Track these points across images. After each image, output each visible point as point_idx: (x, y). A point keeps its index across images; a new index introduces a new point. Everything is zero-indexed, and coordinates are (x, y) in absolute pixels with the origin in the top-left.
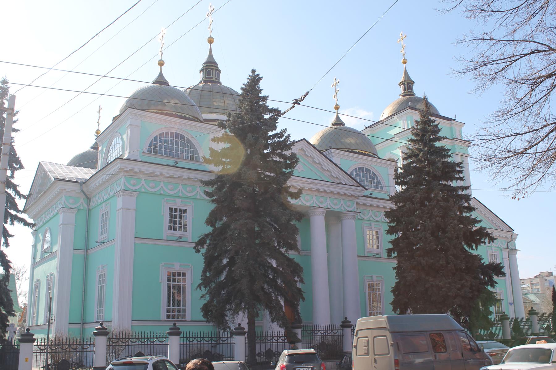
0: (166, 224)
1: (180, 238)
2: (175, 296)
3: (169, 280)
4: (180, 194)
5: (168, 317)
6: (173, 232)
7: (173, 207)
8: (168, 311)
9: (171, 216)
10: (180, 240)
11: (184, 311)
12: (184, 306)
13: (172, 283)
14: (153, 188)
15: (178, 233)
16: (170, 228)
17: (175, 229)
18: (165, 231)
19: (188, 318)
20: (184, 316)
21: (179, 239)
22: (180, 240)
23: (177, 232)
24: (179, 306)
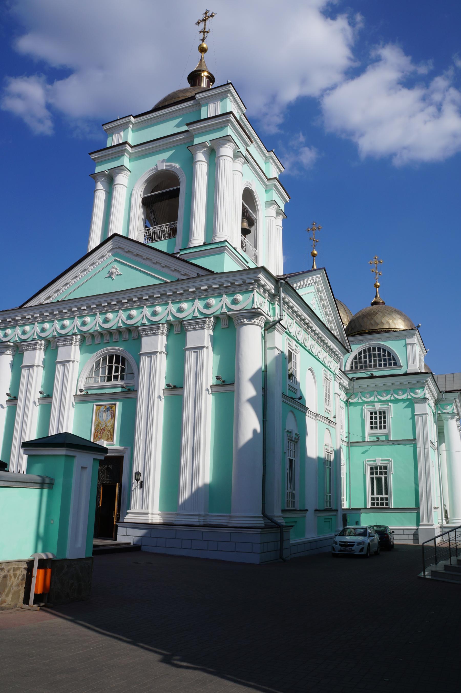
5: (373, 504)
11: (372, 473)
12: (372, 479)
17: (376, 428)
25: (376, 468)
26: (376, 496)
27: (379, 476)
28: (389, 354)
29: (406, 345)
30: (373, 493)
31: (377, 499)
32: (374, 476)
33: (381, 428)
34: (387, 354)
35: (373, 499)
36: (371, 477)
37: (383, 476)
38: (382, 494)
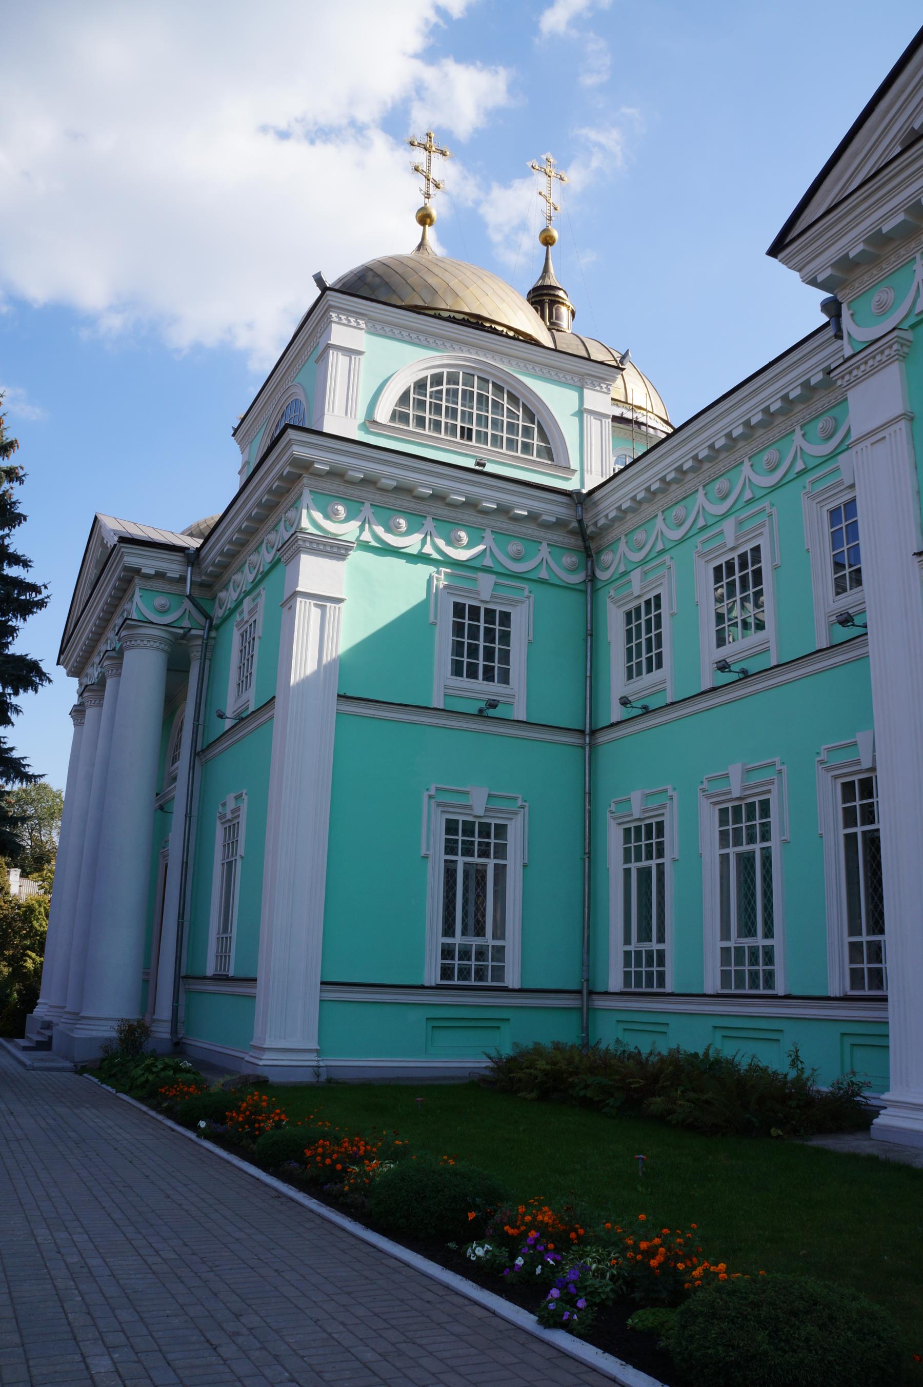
0: (447, 656)
1: (493, 705)
2: (470, 897)
3: (450, 848)
4: (544, 574)
5: (446, 972)
6: (464, 682)
7: (468, 602)
8: (447, 952)
9: (458, 629)
10: (491, 712)
11: (499, 952)
12: (500, 933)
13: (461, 860)
14: (517, 558)
16: (457, 670)
18: (439, 681)
19: (512, 979)
20: (499, 972)
21: (487, 713)
22: (491, 712)
23: (479, 684)
24: (480, 931)
25: (468, 829)
26: (458, 940)
27: (475, 859)
28: (530, 415)
29: (581, 413)
30: (500, 871)
31: (465, 954)
32: (461, 860)
33: (489, 675)
34: (521, 414)
35: (501, 851)
36: (503, 937)
37: (491, 862)
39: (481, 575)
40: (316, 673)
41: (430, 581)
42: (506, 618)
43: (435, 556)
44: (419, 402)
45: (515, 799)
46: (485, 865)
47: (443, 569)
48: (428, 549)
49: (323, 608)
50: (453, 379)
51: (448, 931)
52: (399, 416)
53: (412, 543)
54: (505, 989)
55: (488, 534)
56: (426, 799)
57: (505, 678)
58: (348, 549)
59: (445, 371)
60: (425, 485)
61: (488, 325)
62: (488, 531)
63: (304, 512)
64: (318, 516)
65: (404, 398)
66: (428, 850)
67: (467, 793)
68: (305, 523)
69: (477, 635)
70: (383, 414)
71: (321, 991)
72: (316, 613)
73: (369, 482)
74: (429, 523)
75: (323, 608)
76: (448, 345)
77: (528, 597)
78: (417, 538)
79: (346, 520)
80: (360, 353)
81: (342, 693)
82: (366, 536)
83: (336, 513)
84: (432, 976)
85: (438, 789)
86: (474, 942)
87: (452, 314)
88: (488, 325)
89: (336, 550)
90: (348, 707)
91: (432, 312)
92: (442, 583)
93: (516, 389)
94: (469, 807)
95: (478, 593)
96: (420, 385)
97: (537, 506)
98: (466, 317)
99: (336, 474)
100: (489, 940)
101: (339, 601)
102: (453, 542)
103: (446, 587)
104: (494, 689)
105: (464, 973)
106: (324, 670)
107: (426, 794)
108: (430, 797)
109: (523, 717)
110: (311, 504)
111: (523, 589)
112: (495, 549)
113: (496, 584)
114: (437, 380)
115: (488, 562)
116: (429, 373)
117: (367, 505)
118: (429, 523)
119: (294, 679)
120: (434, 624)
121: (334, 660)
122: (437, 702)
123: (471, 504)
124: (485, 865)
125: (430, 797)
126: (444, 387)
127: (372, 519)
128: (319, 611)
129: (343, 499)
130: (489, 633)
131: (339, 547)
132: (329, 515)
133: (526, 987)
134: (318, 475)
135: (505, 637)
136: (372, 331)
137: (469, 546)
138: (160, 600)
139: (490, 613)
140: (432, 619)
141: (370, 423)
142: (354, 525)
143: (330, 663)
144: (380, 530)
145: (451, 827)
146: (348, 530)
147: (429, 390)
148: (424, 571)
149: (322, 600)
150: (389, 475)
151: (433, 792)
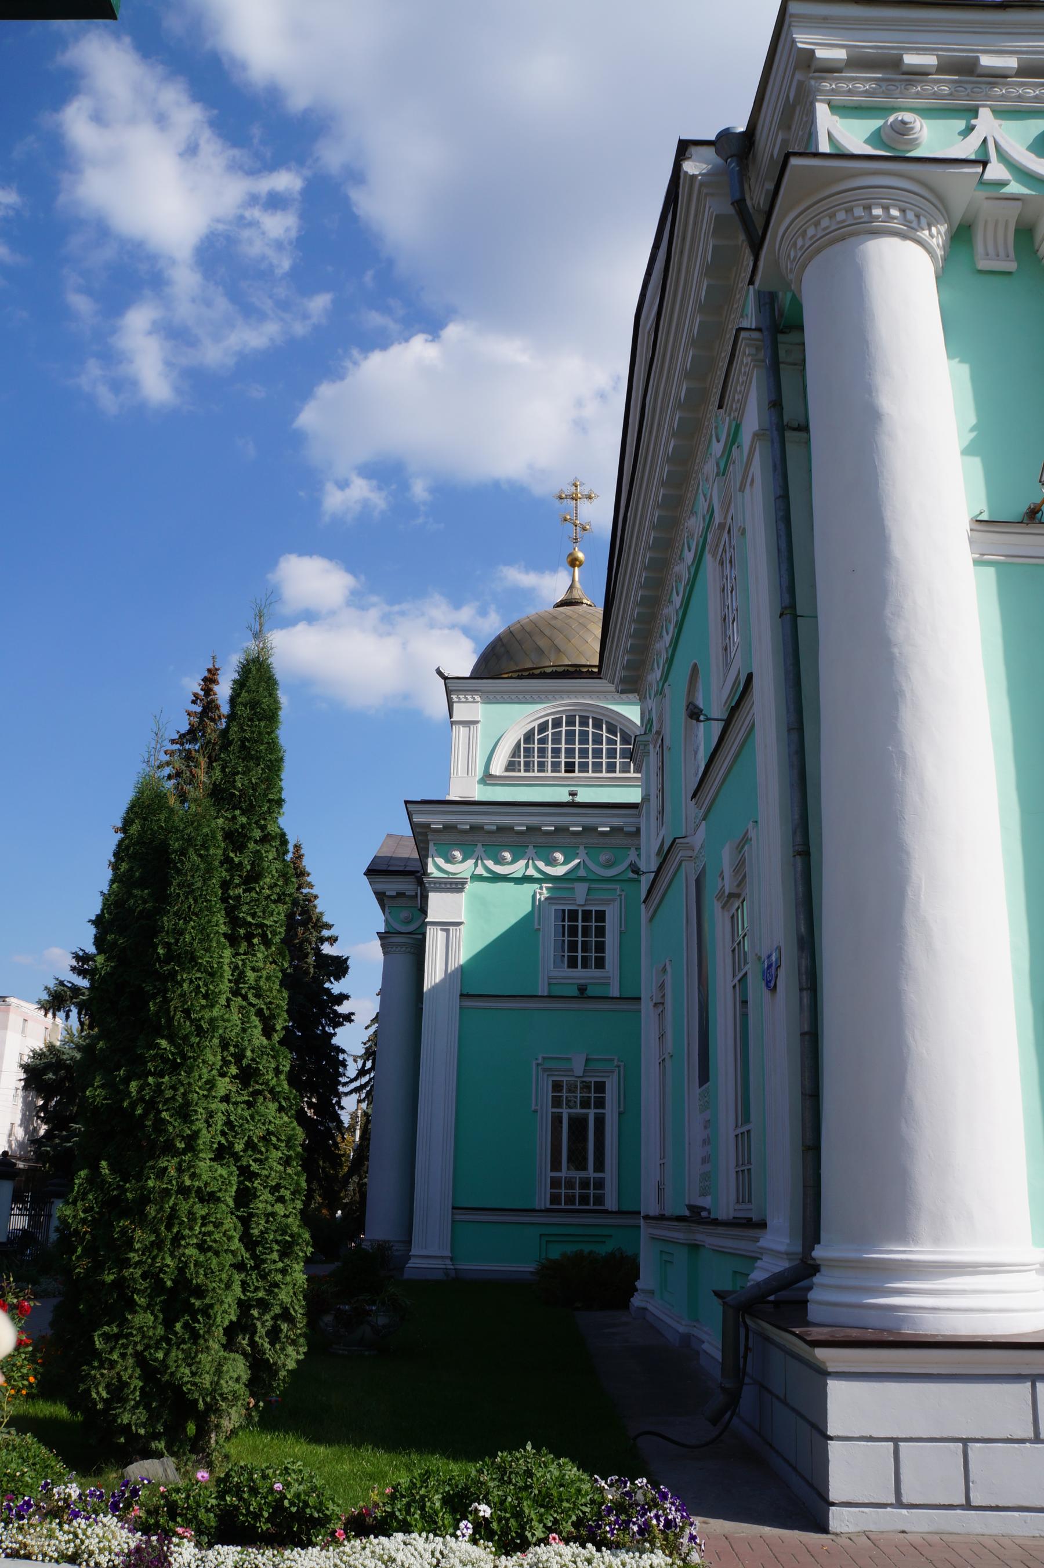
3: (557, 1102)
5: (555, 1199)
7: (567, 908)
8: (555, 1183)
11: (600, 1184)
12: (600, 1166)
14: (609, 865)
15: (580, 974)
18: (548, 968)
19: (611, 1203)
20: (599, 1200)
26: (564, 1173)
30: (600, 1121)
31: (570, 1184)
35: (600, 1103)
37: (591, 1113)
38: (569, 1115)
39: (576, 885)
40: (443, 981)
41: (534, 896)
42: (601, 916)
43: (537, 875)
44: (528, 753)
45: (612, 1060)
46: (587, 1115)
47: (544, 885)
48: (531, 872)
49: (447, 931)
50: (557, 723)
51: (556, 1165)
52: (511, 766)
53: (518, 868)
54: (606, 1212)
55: (582, 850)
56: (534, 1066)
57: (600, 963)
58: (464, 883)
59: (550, 718)
60: (520, 822)
61: (585, 670)
62: (582, 848)
63: (430, 860)
64: (440, 861)
65: (516, 752)
66: (536, 1105)
67: (569, 1059)
68: (431, 869)
69: (577, 929)
70: (498, 768)
71: (453, 1214)
72: (441, 935)
73: (475, 829)
74: (531, 850)
75: (447, 931)
76: (550, 697)
77: (620, 896)
78: (522, 863)
79: (464, 860)
80: (477, 722)
81: (465, 992)
82: (480, 871)
83: (454, 857)
84: (542, 1201)
85: (544, 1058)
86: (578, 1175)
87: (554, 669)
88: (585, 670)
89: (455, 886)
90: (468, 1003)
91: (537, 672)
92: (545, 893)
93: (613, 719)
94: (571, 1070)
95: (574, 899)
96: (529, 737)
97: (617, 822)
98: (566, 668)
99: (449, 828)
100: (591, 1173)
101: (459, 924)
102: (551, 862)
103: (547, 899)
104: (593, 973)
105: (570, 1200)
106: (449, 977)
107: (534, 1063)
108: (538, 1065)
109: (616, 994)
110: (435, 853)
111: (615, 889)
112: (588, 862)
113: (589, 889)
114: (543, 728)
115: (582, 873)
116: (536, 724)
117: (480, 846)
118: (531, 850)
119: (425, 989)
120: (539, 929)
121: (456, 969)
122: (542, 990)
123: (561, 830)
124: (587, 1115)
125: (538, 1065)
126: (550, 732)
127: (484, 855)
128: (444, 933)
129: (459, 845)
130: (586, 931)
131: (457, 883)
132: (450, 860)
133: (624, 1208)
134: (436, 831)
135: (601, 932)
136: (487, 701)
137: (565, 863)
138: (404, 914)
139: (587, 915)
140: (536, 926)
141: (488, 779)
142: (471, 862)
143: (453, 972)
144: (490, 863)
145: (557, 1086)
146: (463, 868)
147: (536, 737)
148: (529, 888)
149: (445, 926)
150: (490, 821)
151: (540, 1061)
